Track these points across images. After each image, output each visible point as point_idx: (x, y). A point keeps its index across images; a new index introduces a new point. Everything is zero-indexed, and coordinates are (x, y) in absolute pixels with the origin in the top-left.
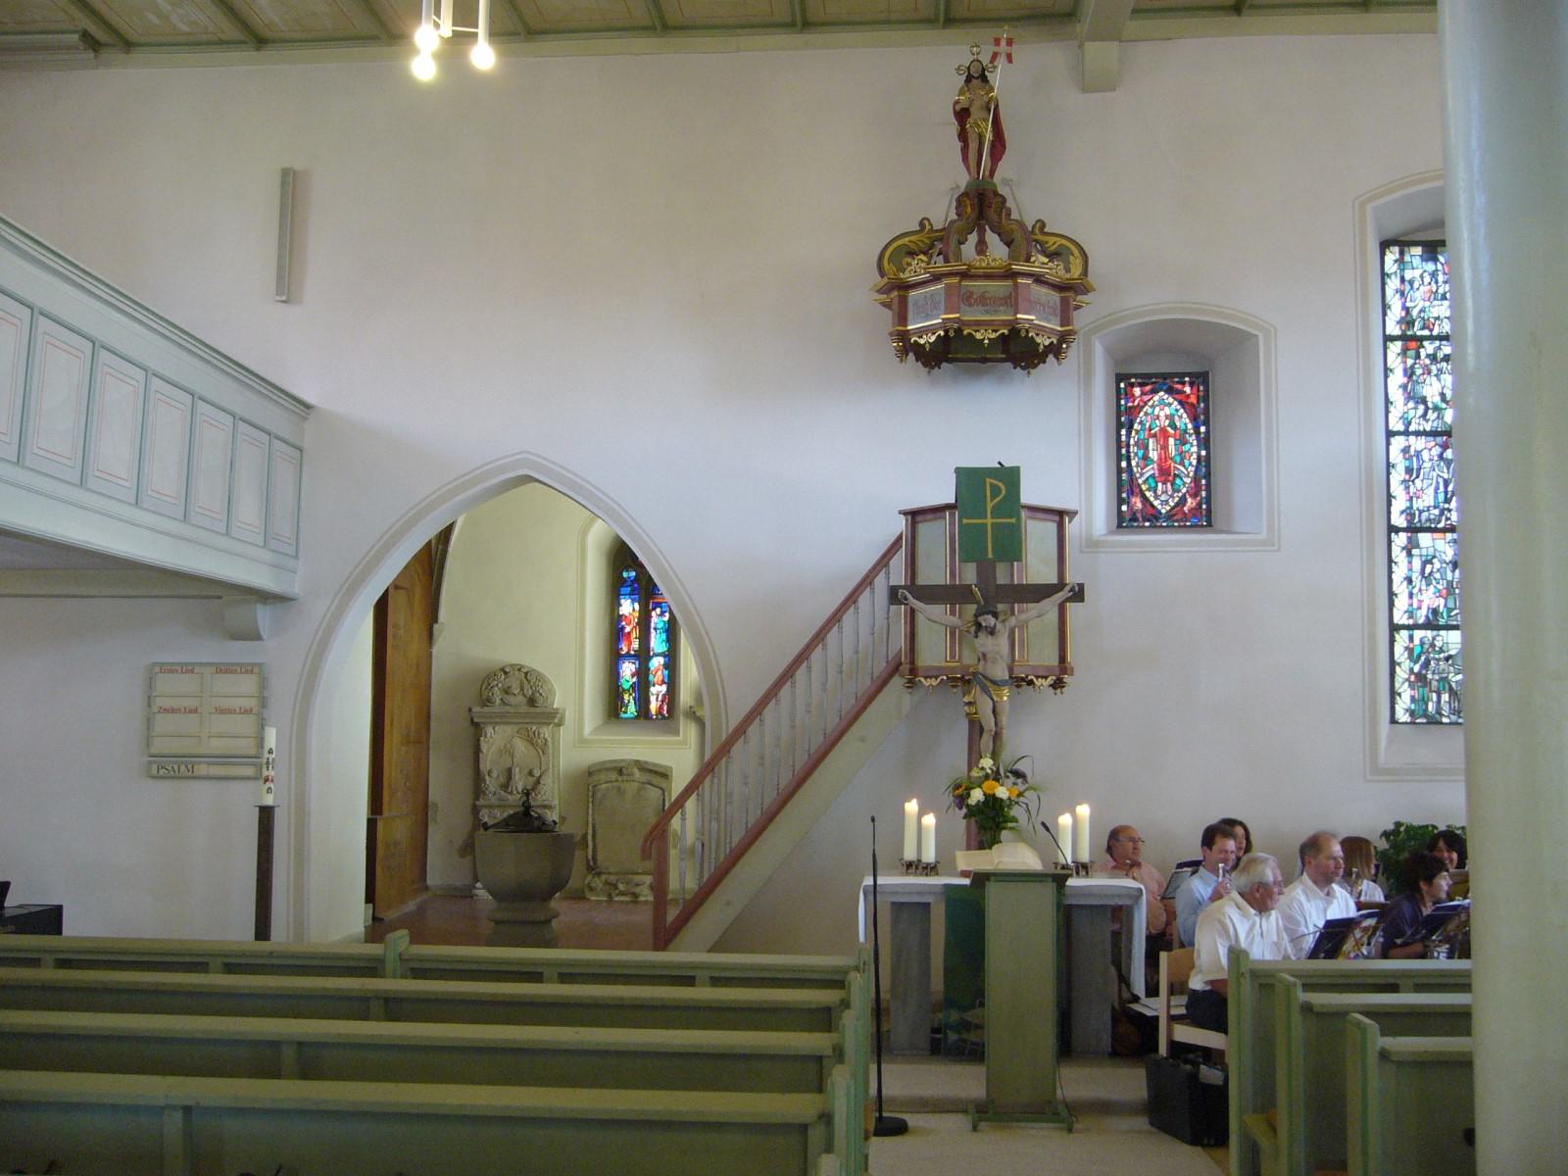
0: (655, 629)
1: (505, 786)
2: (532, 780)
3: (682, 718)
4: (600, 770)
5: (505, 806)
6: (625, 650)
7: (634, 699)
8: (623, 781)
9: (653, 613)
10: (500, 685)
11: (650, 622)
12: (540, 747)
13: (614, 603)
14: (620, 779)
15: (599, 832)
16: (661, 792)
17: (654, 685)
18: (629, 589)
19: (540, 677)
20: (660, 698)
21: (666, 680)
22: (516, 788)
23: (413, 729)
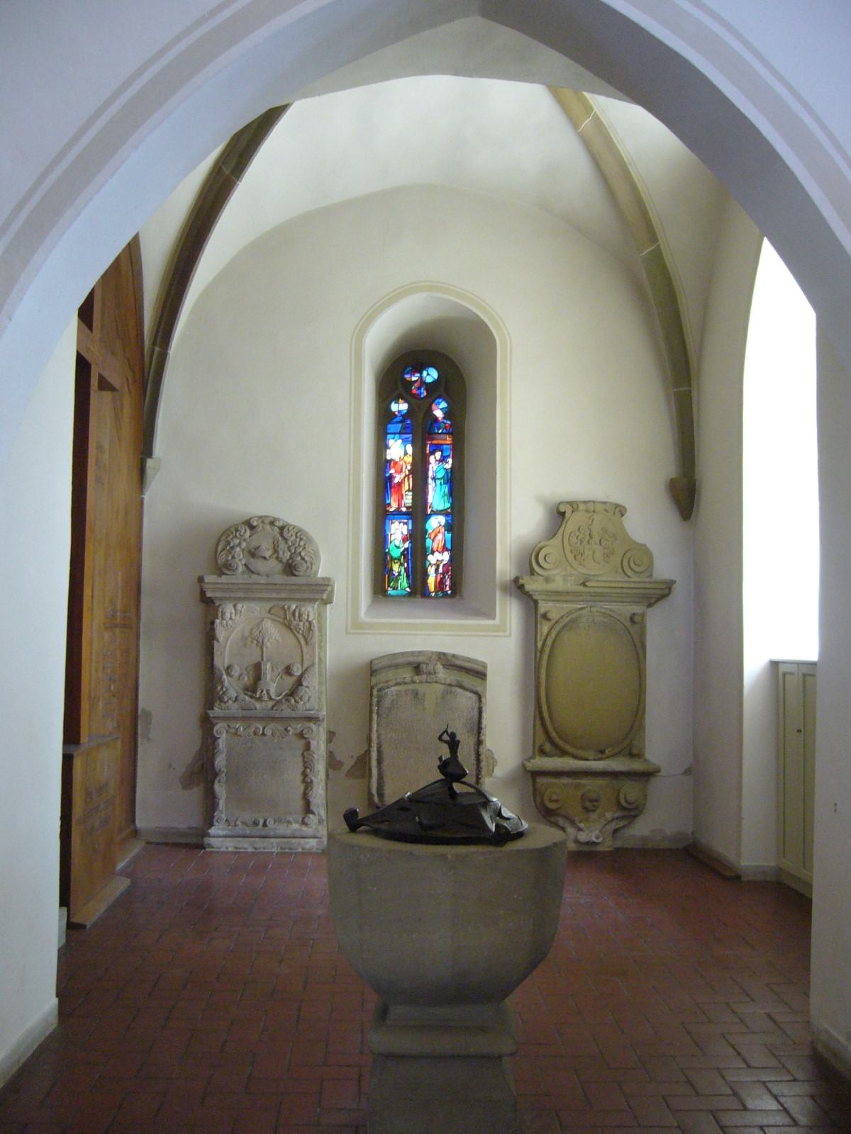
0: (434, 479)
1: (252, 689)
2: (289, 681)
3: (498, 593)
4: (389, 667)
5: (249, 718)
6: (394, 506)
7: (407, 570)
8: (421, 682)
9: (432, 459)
10: (244, 545)
11: (428, 470)
12: (304, 633)
13: (381, 445)
14: (417, 678)
15: (386, 750)
16: (474, 697)
17: (433, 553)
18: (400, 425)
19: (300, 534)
20: (441, 570)
21: (449, 546)
22: (268, 692)
23: (119, 605)
